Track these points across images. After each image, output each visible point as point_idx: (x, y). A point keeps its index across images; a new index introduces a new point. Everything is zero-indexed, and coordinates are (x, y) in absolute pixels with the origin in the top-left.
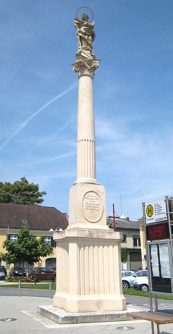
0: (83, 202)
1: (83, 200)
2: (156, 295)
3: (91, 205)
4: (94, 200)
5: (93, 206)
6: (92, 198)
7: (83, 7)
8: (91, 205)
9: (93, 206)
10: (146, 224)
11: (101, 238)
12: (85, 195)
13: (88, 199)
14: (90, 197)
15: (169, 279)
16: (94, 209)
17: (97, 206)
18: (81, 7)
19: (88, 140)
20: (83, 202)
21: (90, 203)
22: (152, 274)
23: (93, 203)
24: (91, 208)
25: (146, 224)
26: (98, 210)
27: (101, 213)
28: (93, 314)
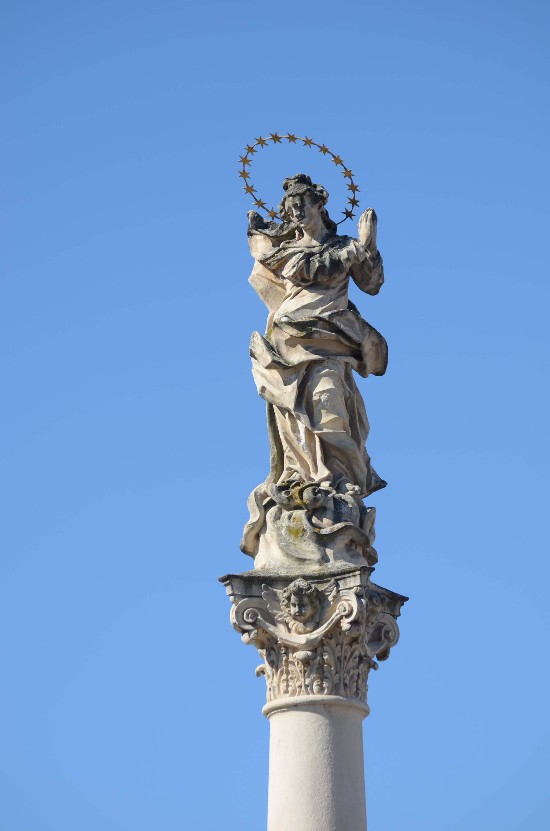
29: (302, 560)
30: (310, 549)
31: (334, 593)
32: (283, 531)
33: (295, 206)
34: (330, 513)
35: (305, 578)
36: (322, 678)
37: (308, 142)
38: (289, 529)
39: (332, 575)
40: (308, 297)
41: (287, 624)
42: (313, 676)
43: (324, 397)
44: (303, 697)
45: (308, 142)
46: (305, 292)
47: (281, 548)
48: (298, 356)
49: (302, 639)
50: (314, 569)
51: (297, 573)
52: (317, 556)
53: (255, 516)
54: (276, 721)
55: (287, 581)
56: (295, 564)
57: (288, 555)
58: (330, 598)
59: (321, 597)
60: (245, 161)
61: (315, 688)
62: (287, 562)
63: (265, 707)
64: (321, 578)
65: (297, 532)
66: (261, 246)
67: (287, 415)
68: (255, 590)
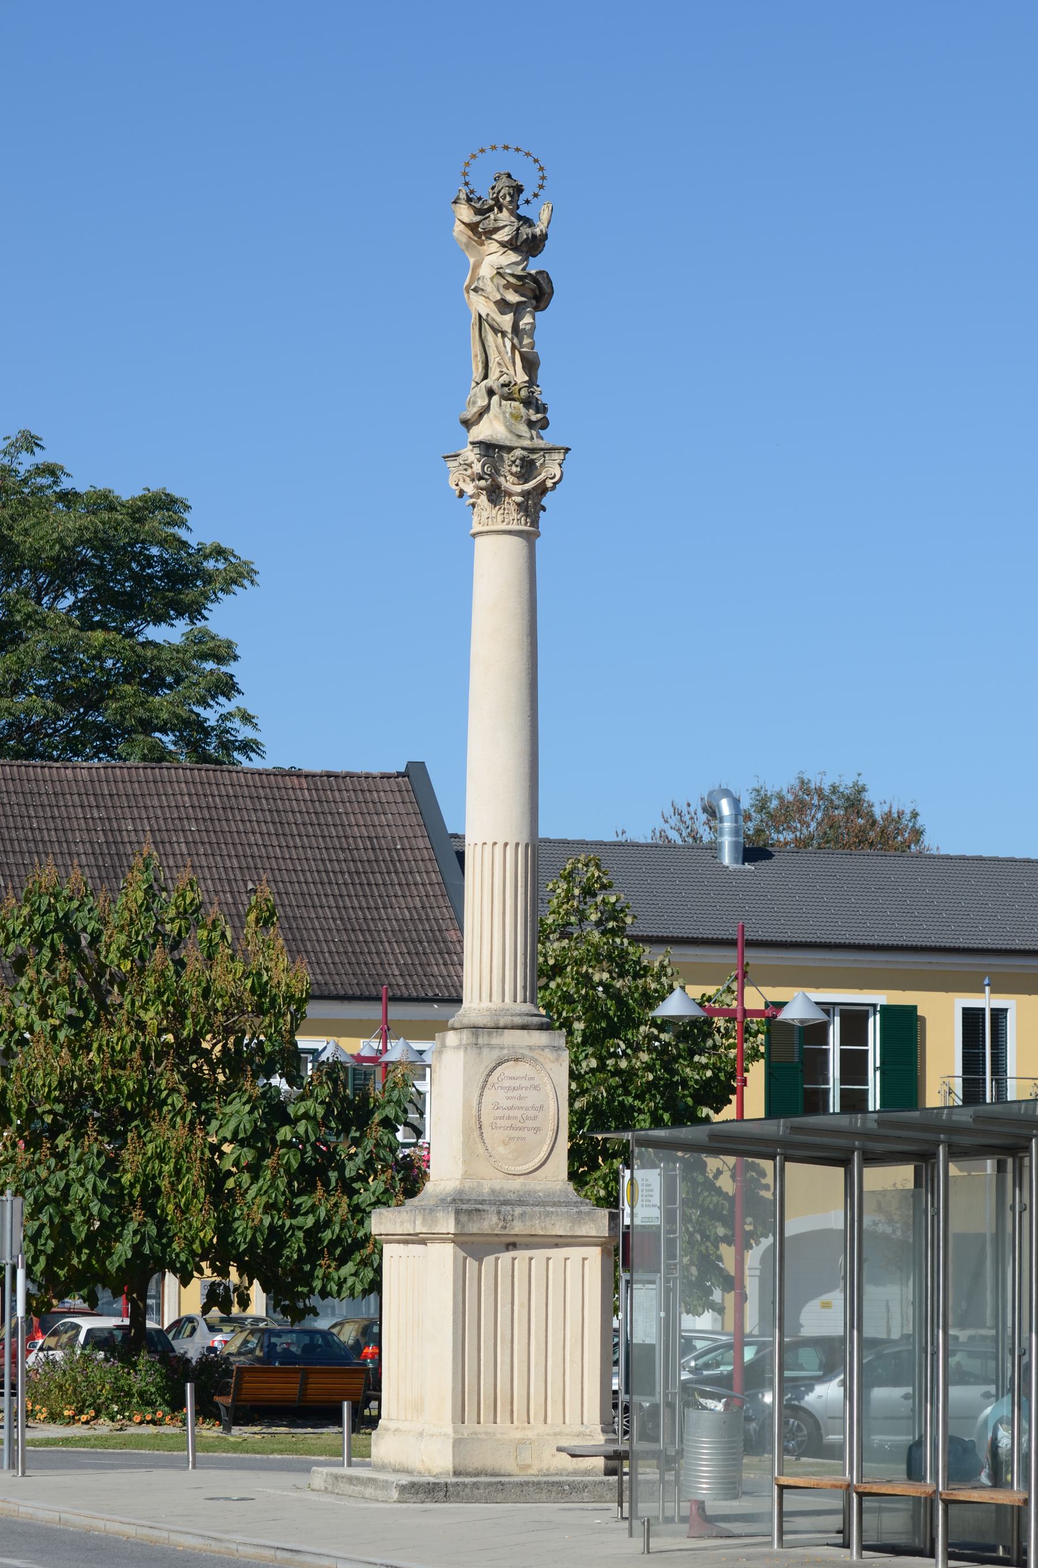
0: (480, 1103)
1: (481, 1095)
2: (678, 1121)
3: (512, 1113)
4: (523, 1093)
5: (518, 1113)
6: (517, 1083)
7: (494, 148)
8: (512, 1113)
9: (518, 1113)
10: (719, 1328)
11: (542, 1233)
12: (489, 1075)
13: (500, 1091)
14: (507, 1083)
15: (652, 1347)
16: (520, 1125)
17: (531, 1113)
18: (487, 147)
19: (495, 844)
20: (480, 1103)
21: (510, 1103)
22: (733, 1121)
23: (517, 1103)
24: (509, 1123)
25: (719, 1328)
26: (537, 1130)
27: (548, 1142)
28: (512, 1479)
29: (520, 436)
30: (523, 429)
31: (541, 461)
32: (507, 415)
33: (509, 194)
34: (533, 407)
35: (523, 449)
36: (527, 516)
37: (518, 150)
38: (511, 414)
39: (542, 449)
40: (513, 257)
41: (505, 477)
42: (522, 514)
43: (528, 327)
44: (515, 527)
45: (518, 150)
46: (510, 252)
47: (507, 427)
48: (513, 298)
49: (518, 489)
50: (527, 443)
51: (516, 445)
52: (528, 435)
53: (482, 402)
54: (479, 541)
55: (510, 449)
56: (515, 438)
57: (511, 432)
58: (538, 464)
59: (532, 462)
60: (543, 178)
61: (523, 522)
62: (509, 436)
63: (473, 531)
64: (533, 450)
65: (516, 417)
66: (465, 213)
67: (499, 335)
68: (491, 452)
